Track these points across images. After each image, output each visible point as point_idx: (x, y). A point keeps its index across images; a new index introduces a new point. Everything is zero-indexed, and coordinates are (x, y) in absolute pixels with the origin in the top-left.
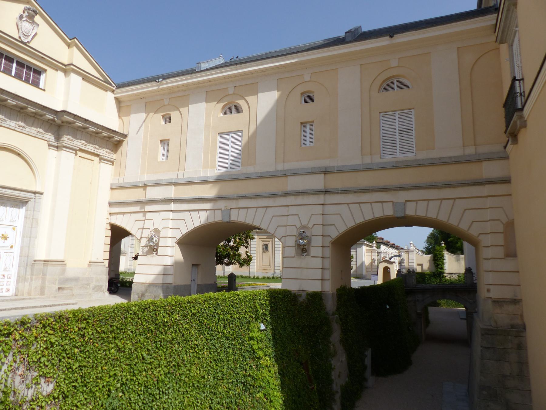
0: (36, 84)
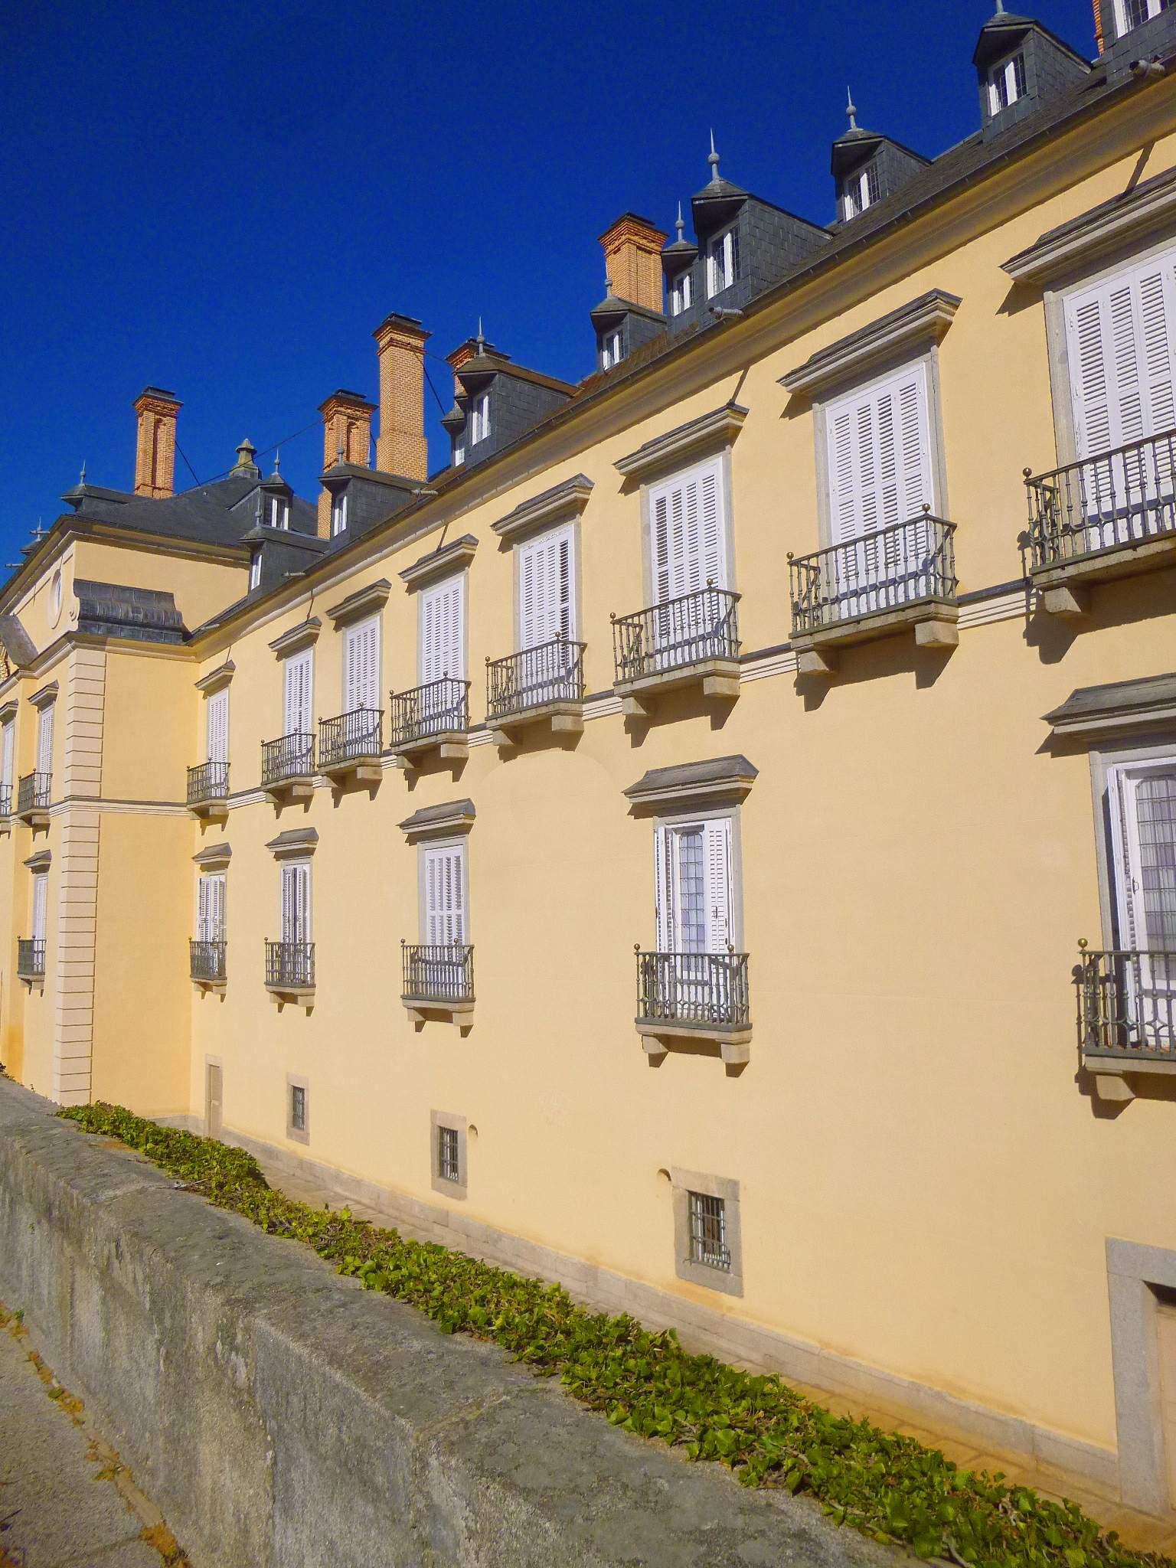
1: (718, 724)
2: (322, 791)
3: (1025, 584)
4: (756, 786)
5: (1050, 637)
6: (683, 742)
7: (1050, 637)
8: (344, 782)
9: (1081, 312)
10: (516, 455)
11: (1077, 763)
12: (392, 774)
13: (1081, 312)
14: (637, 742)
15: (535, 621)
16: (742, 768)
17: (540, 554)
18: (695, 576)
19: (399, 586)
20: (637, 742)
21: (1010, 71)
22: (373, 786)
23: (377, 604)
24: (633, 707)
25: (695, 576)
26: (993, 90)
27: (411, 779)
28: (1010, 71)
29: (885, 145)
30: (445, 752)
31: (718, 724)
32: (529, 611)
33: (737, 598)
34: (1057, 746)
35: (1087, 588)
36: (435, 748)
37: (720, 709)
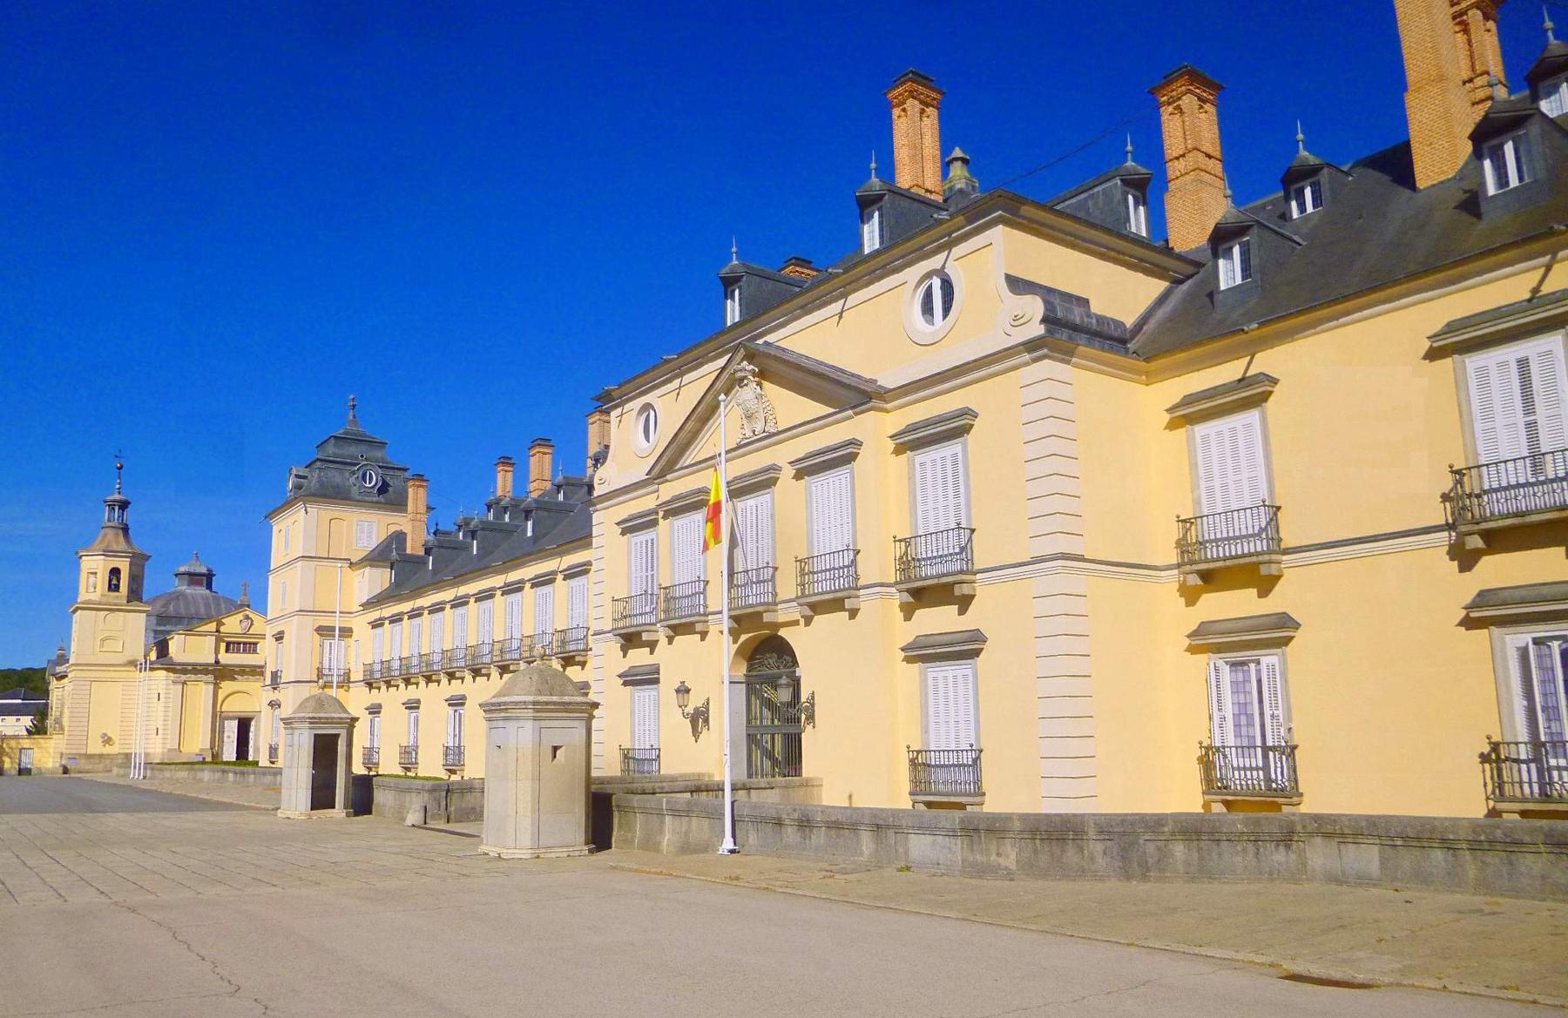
0: (255, 651)
1: (962, 611)
2: (468, 677)
3: (1449, 527)
4: (1299, 634)
5: (1190, 596)
6: (939, 620)
7: (1465, 559)
8: (476, 672)
9: (1203, 437)
10: (216, 798)
11: (1481, 634)
12: (495, 673)
13: (1203, 437)
14: (908, 618)
15: (941, 510)
16: (977, 637)
17: (1219, 433)
18: (947, 517)
19: (788, 472)
20: (908, 618)
21: (1308, 192)
22: (439, 682)
23: (770, 483)
24: (907, 598)
25: (947, 517)
26: (1294, 204)
27: (625, 651)
28: (1308, 192)
29: (268, 764)
30: (645, 637)
31: (962, 611)
32: (925, 503)
33: (973, 531)
34: (1469, 623)
35: (1487, 535)
36: (639, 634)
37: (964, 603)
